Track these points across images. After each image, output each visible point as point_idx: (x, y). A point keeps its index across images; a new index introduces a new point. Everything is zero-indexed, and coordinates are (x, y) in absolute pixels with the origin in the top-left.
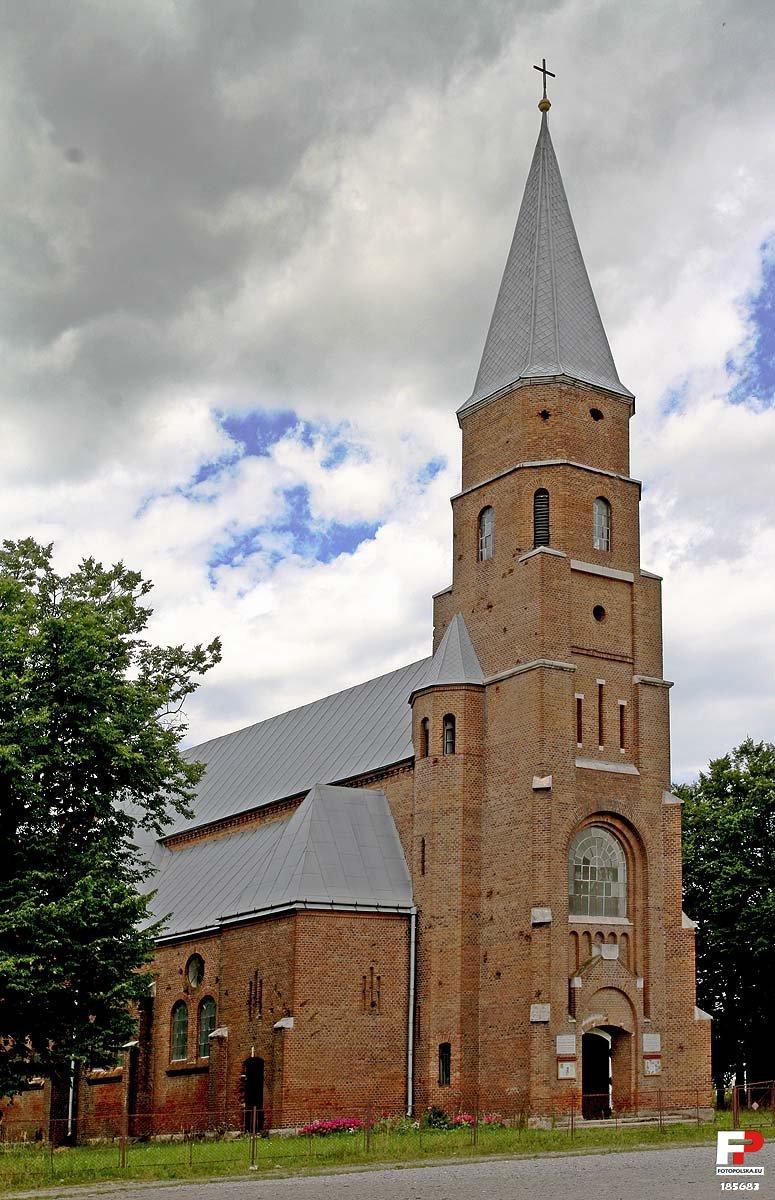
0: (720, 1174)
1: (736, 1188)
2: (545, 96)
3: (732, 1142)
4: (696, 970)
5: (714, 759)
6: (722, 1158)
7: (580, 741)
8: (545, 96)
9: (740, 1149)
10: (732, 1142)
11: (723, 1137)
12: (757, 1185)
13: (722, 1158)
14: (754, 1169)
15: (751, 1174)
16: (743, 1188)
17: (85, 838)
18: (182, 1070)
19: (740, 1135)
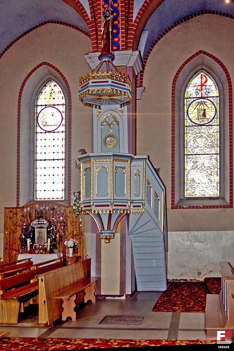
0: (218, 343)
1: (223, 348)
2: (61, 132)
3: (221, 334)
4: (183, 18)
5: (1, 289)
6: (219, 339)
7: (85, 171)
8: (61, 132)
9: (224, 336)
10: (221, 334)
11: (219, 333)
12: (229, 347)
13: (219, 339)
14: (228, 342)
15: (227, 343)
16: (225, 347)
17: (23, 247)
18: (147, 330)
19: (224, 332)
